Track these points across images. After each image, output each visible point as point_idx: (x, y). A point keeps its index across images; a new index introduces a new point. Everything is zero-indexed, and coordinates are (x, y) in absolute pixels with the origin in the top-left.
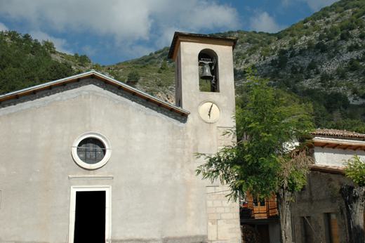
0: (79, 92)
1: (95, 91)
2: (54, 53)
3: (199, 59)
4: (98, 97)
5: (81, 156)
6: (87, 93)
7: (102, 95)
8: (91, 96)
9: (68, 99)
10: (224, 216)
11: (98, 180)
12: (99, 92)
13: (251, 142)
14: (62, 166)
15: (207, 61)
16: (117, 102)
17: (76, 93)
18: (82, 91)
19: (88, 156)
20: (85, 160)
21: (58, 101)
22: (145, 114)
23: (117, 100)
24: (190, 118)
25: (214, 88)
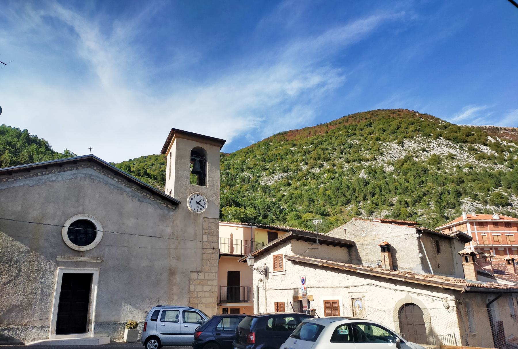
0: (75, 174)
1: (92, 175)
2: (167, 209)
3: (192, 155)
4: (94, 180)
5: (71, 237)
6: (83, 176)
7: (98, 179)
8: (87, 179)
9: (63, 180)
10: (204, 300)
11: (85, 264)
12: (95, 176)
13: (354, 134)
14: (51, 247)
15: (198, 158)
16: (112, 187)
17: (73, 175)
18: (79, 173)
19: (79, 238)
20: (74, 241)
21: (53, 181)
22: (139, 201)
23: (112, 185)
24: (280, 300)
25: (202, 182)
